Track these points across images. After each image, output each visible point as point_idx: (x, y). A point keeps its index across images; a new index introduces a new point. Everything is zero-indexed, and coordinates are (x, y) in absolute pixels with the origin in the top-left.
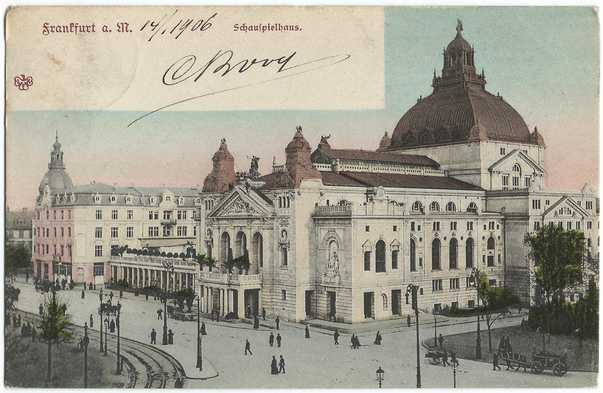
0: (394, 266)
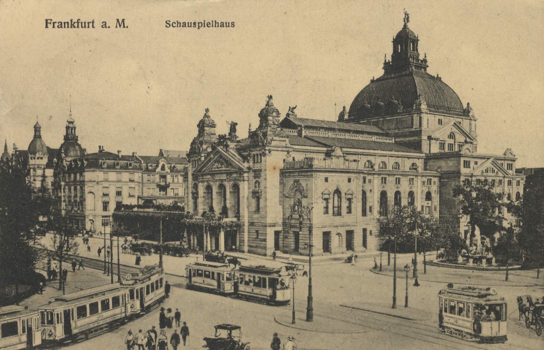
0: (350, 212)
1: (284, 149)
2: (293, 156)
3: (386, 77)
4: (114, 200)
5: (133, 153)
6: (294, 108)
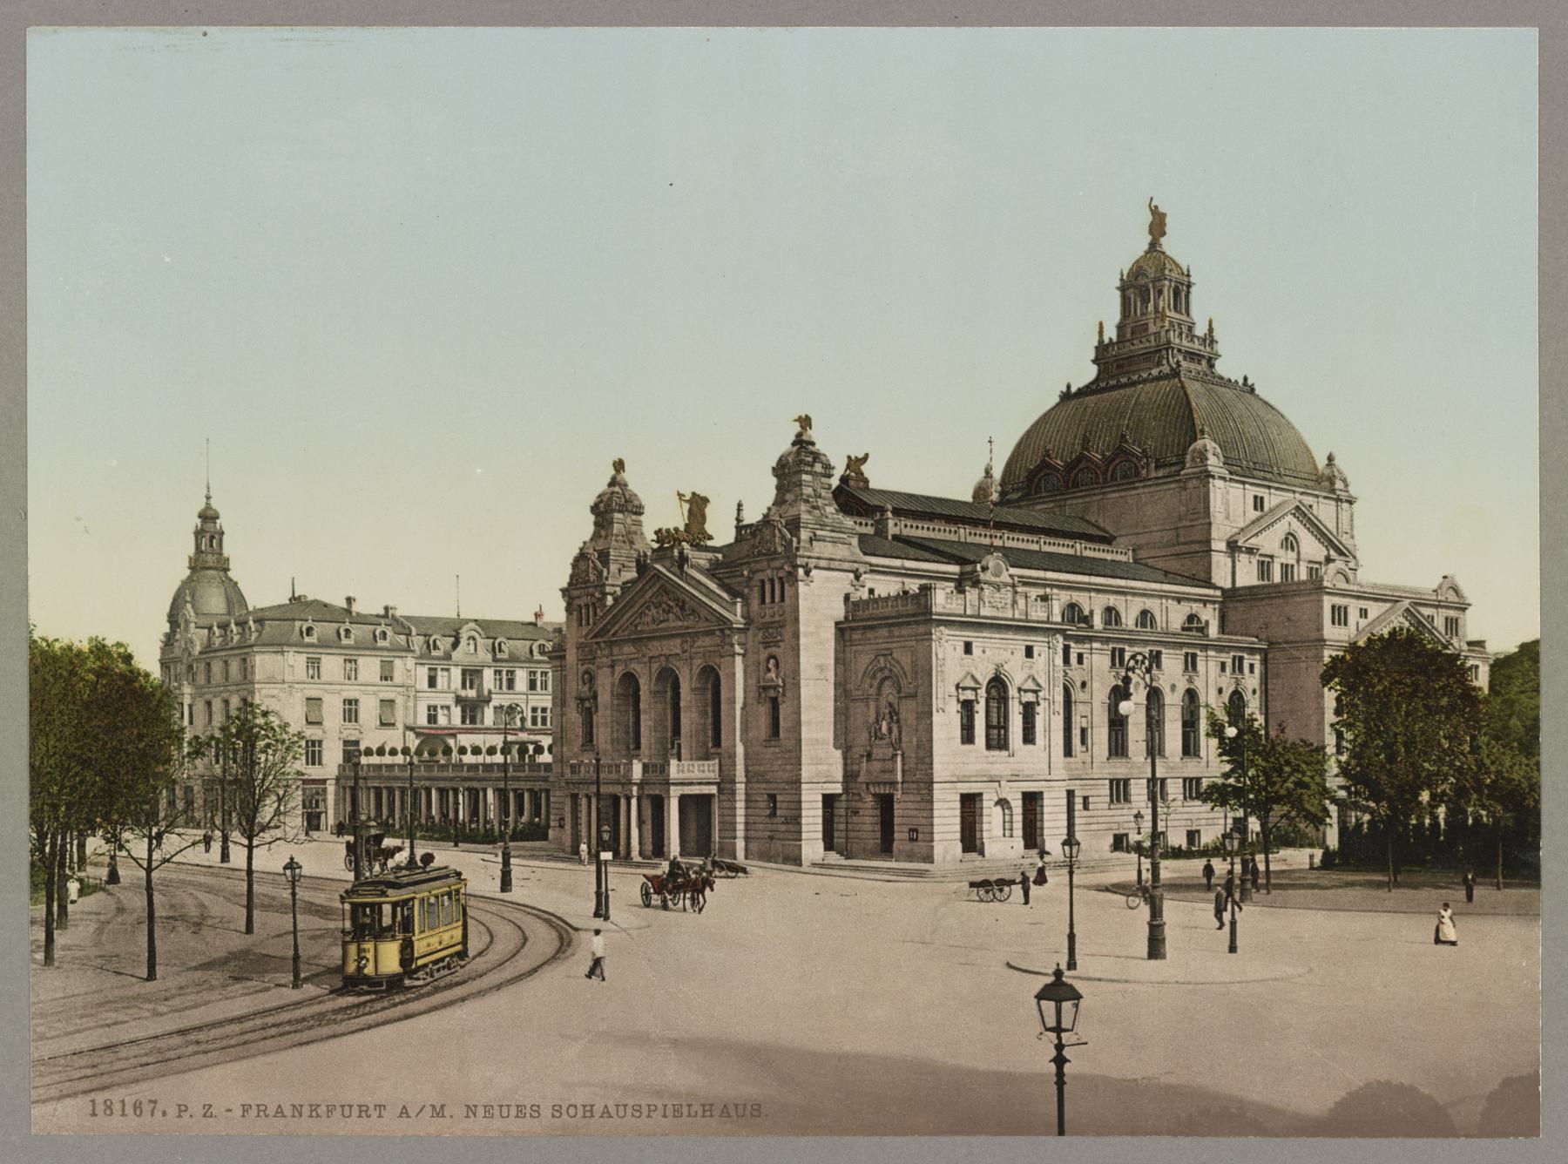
0: (1029, 737)
1: (846, 566)
2: (869, 585)
4: (336, 735)
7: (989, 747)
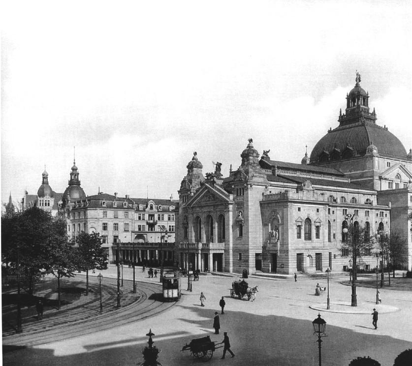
0: (318, 236)
1: (264, 184)
3: (341, 128)
5: (126, 196)
6: (268, 152)
7: (305, 239)
